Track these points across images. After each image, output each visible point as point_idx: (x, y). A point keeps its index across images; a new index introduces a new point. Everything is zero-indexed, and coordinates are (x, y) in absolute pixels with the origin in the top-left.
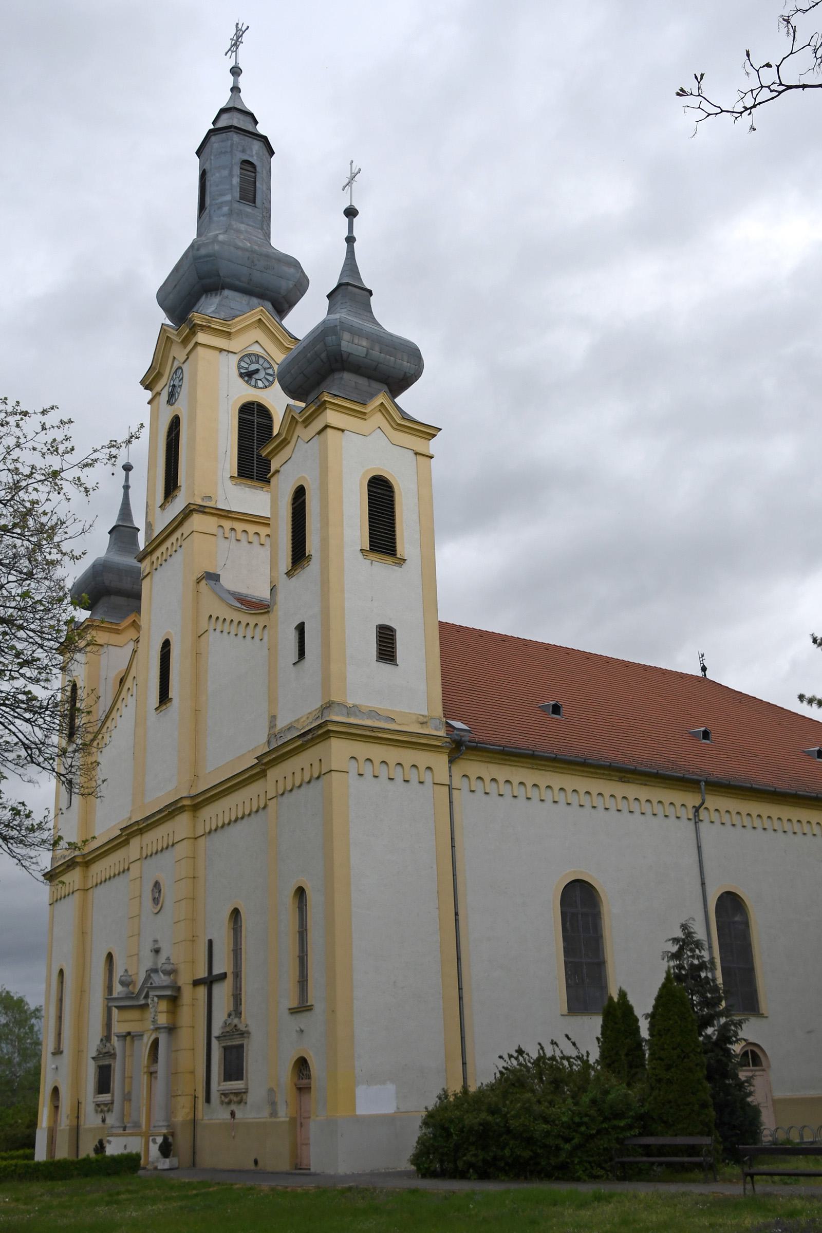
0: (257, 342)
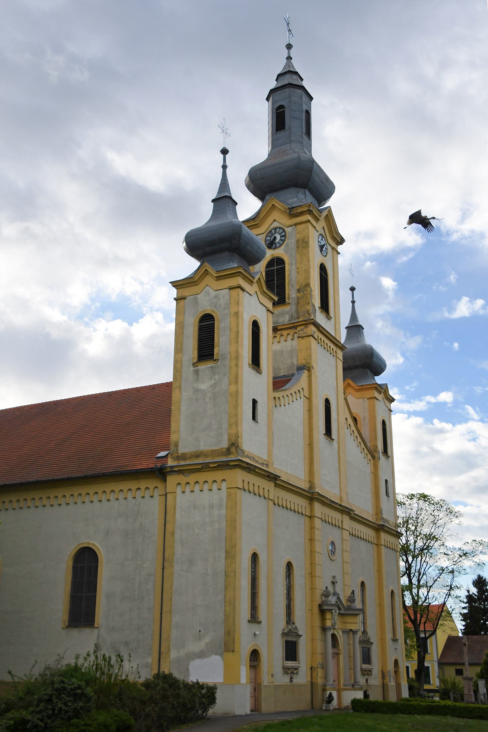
0: (275, 220)
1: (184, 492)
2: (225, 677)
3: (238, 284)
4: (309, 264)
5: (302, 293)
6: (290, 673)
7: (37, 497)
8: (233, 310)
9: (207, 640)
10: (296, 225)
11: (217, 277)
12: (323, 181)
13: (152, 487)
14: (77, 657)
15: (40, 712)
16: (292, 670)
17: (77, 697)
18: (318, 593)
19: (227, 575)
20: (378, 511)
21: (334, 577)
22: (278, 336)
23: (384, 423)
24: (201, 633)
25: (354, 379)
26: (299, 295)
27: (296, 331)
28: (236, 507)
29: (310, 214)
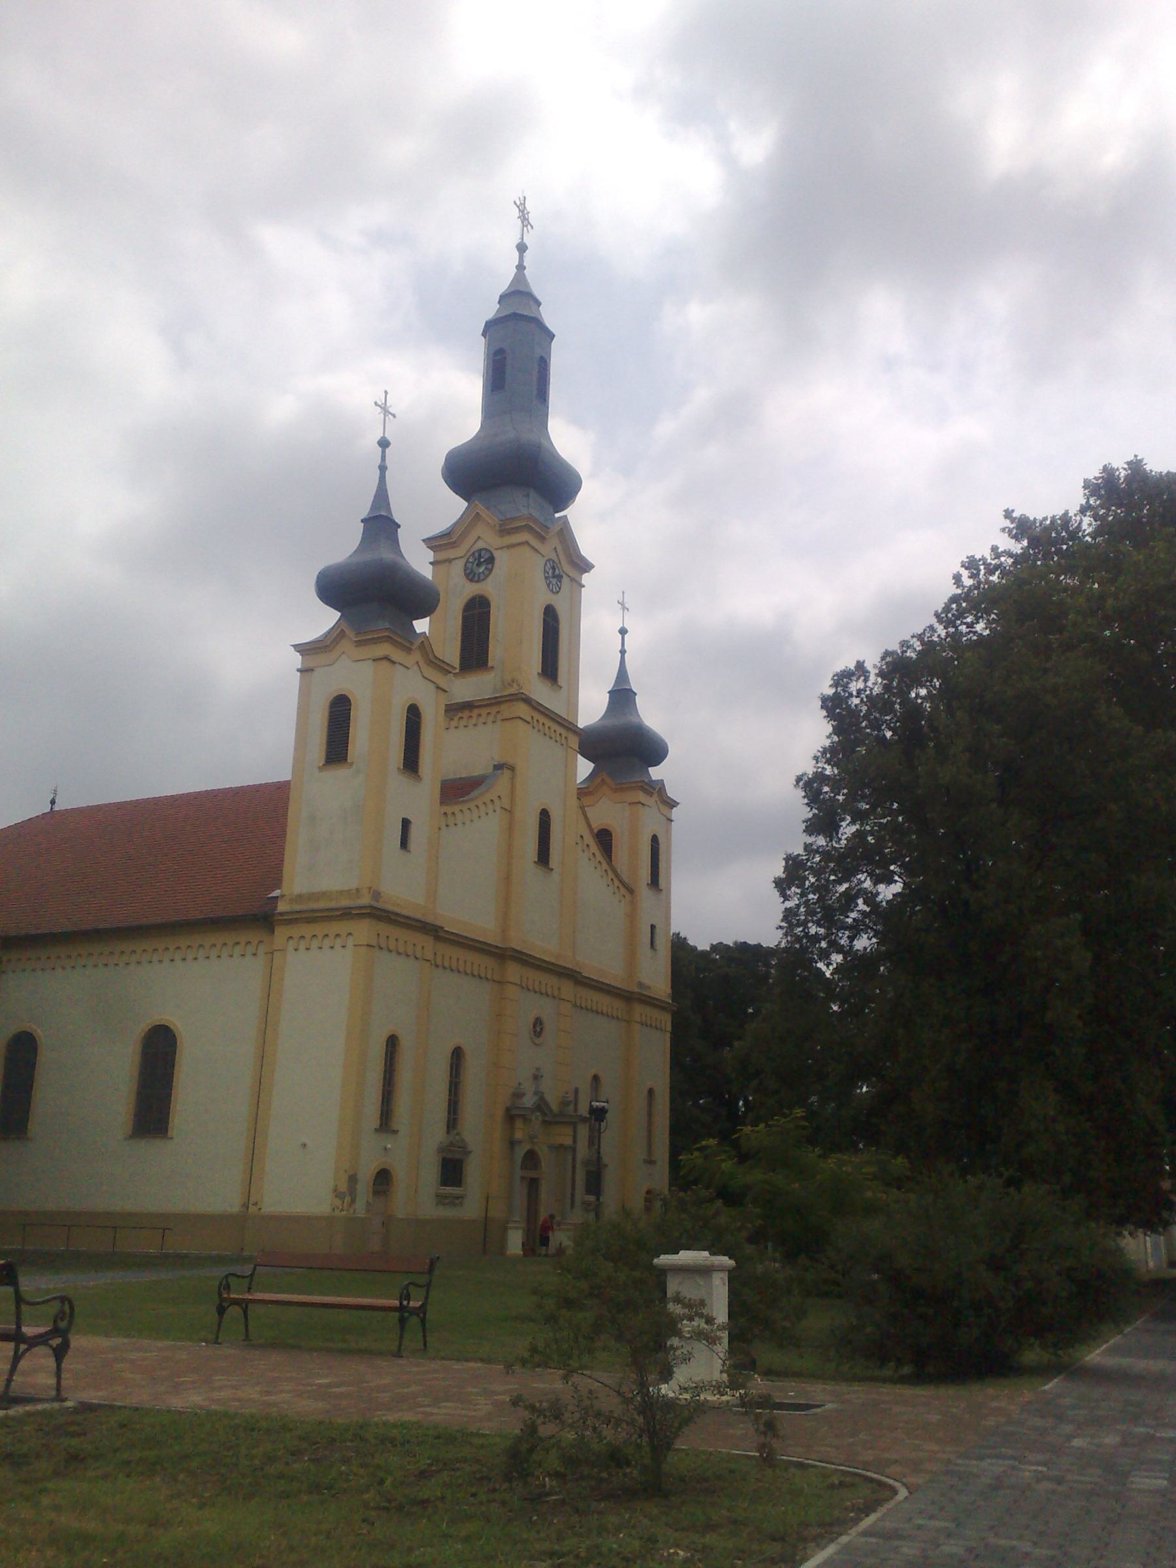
0: (479, 537)
21: (538, 1069)
23: (655, 839)
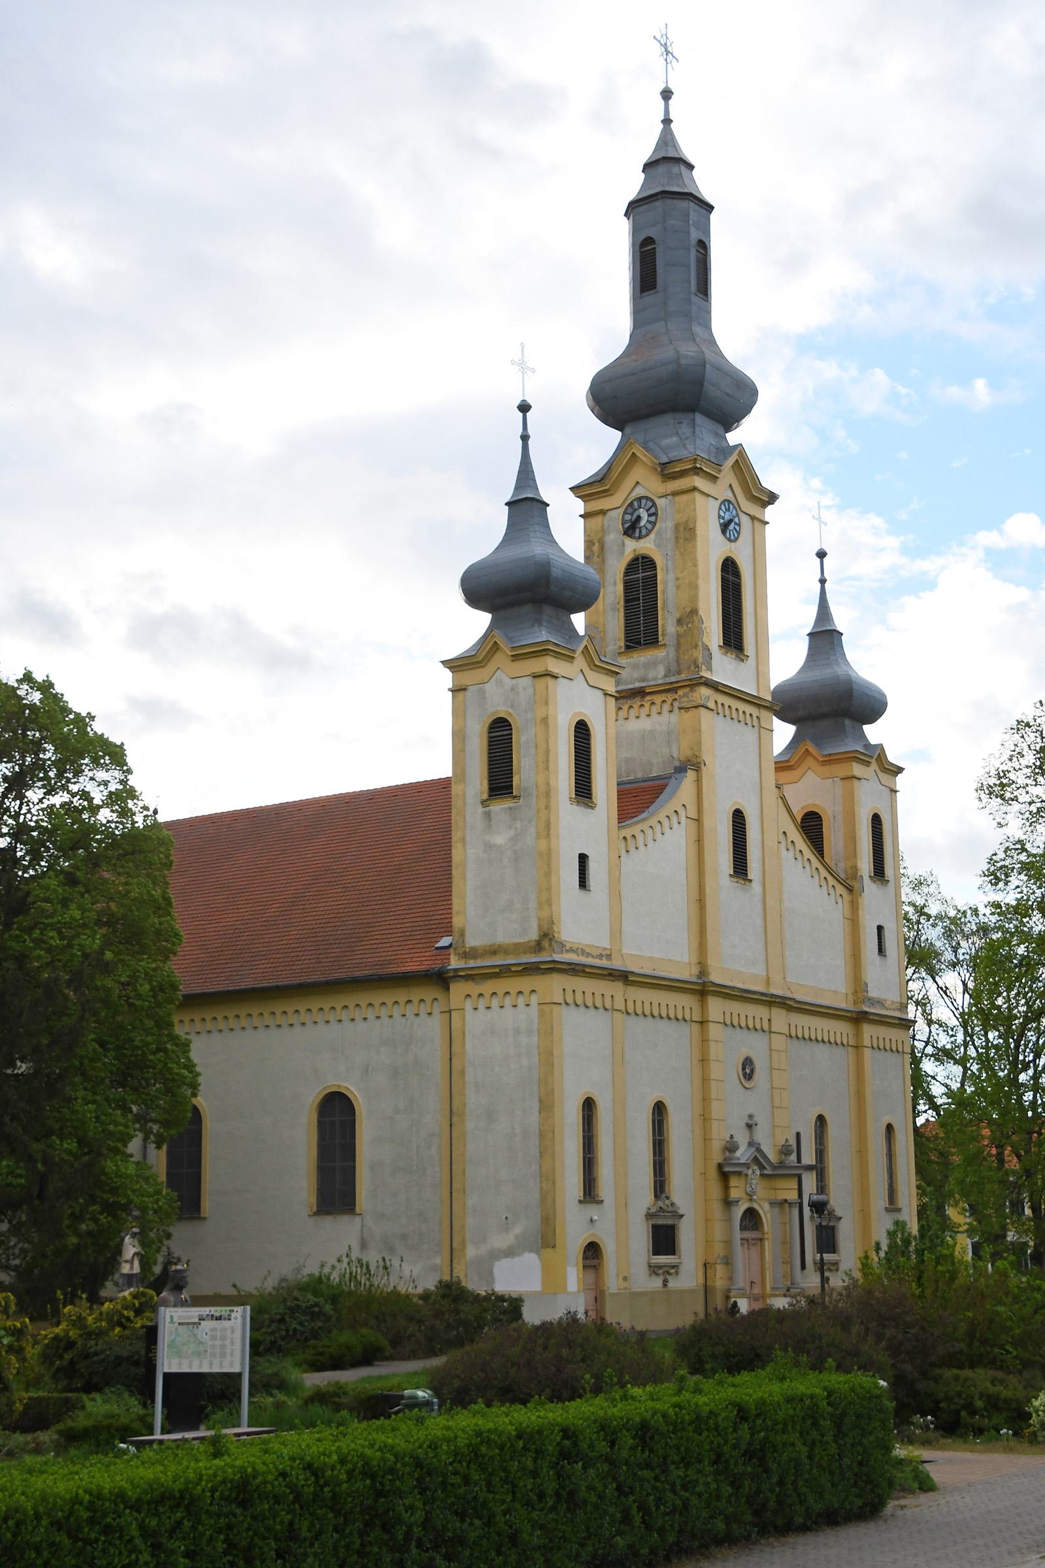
0: (638, 483)
1: (476, 1009)
2: (544, 1284)
3: (544, 669)
4: (697, 572)
5: (685, 627)
6: (663, 1273)
7: (255, 1012)
8: (540, 713)
9: (517, 1230)
10: (675, 494)
11: (512, 656)
12: (730, 392)
13: (429, 999)
14: (322, 1266)
15: (272, 1333)
16: (666, 1269)
17: (314, 1316)
18: (717, 1145)
19: (542, 1136)
20: (858, 985)
21: (751, 1116)
22: (647, 705)
23: (876, 820)
24: (509, 1221)
25: (818, 741)
26: (681, 630)
27: (676, 696)
28: (552, 1033)
29: (697, 474)
